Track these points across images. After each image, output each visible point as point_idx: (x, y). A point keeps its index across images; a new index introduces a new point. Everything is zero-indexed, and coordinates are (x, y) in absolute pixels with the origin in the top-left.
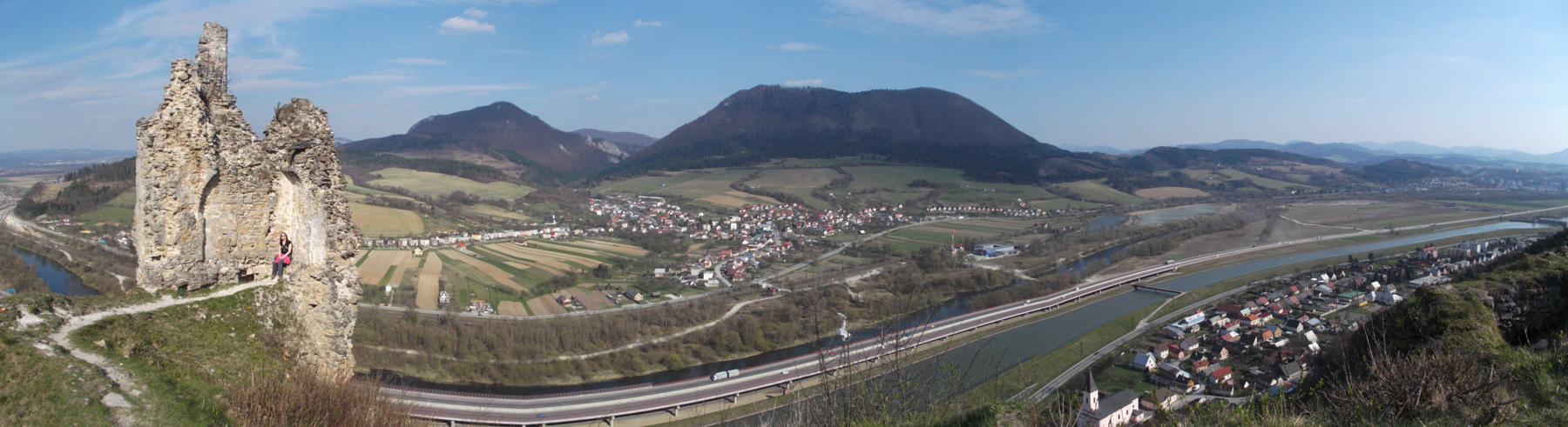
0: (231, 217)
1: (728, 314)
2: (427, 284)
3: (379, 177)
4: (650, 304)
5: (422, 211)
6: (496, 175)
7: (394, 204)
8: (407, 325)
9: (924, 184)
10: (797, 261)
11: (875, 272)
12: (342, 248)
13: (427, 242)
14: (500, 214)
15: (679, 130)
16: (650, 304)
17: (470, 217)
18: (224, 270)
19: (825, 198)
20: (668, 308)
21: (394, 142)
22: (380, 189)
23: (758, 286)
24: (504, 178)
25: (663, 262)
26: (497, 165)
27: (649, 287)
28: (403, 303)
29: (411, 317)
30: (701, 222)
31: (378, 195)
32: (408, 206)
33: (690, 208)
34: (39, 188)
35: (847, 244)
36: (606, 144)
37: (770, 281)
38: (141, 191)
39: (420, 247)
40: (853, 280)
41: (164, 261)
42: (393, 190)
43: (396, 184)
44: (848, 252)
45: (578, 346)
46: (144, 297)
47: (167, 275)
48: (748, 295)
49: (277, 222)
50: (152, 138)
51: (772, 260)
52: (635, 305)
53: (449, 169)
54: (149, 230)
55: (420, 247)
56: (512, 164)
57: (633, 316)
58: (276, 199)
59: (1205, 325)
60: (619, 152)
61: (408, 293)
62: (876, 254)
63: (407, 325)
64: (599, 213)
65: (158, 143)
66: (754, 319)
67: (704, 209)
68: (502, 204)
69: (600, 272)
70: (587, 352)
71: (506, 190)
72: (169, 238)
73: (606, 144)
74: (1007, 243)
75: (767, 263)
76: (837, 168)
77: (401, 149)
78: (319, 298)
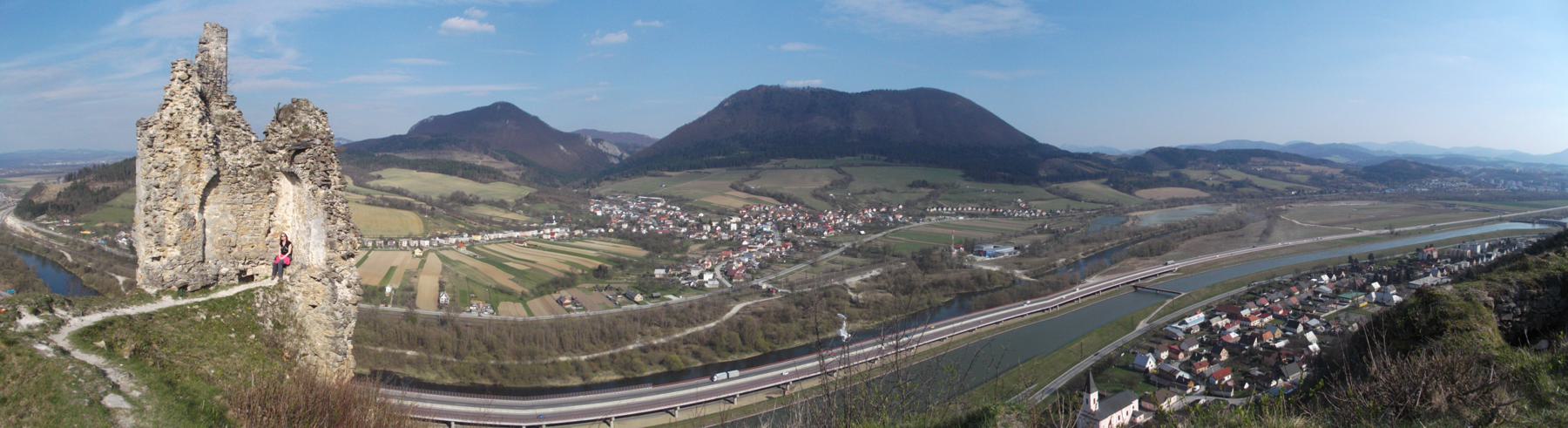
0: (231, 217)
1: (728, 315)
2: (427, 285)
3: (379, 177)
4: (650, 305)
5: (422, 211)
6: (496, 176)
7: (394, 205)
8: (406, 326)
9: (924, 184)
10: (797, 262)
11: (875, 272)
12: (342, 249)
13: (427, 243)
14: (500, 214)
15: (679, 130)
16: (650, 305)
17: (471, 218)
18: (224, 270)
19: (825, 199)
20: (668, 309)
21: (394, 143)
22: (380, 189)
23: (758, 287)
24: (505, 179)
25: (663, 262)
26: (497, 166)
27: (649, 288)
28: (403, 304)
29: (411, 318)
30: (701, 223)
31: (377, 195)
32: (408, 207)
33: (690, 209)
34: (38, 189)
35: (847, 245)
36: (606, 144)
37: (770, 282)
38: (141, 192)
39: (420, 247)
40: (853, 281)
41: (164, 261)
42: (393, 191)
43: (396, 184)
44: (848, 252)
45: (578, 347)
46: (144, 298)
47: (167, 275)
48: (748, 296)
49: (277, 222)
50: (152, 138)
51: (771, 260)
52: (635, 306)
53: (449, 169)
54: (149, 230)
55: (420, 247)
56: (512, 165)
57: (633, 317)
58: (276, 200)
59: (1205, 326)
60: (619, 153)
61: (408, 294)
62: (876, 255)
63: (406, 326)
64: (599, 213)
65: (158, 143)
66: (755, 320)
67: (705, 210)
68: (502, 205)
69: (600, 273)
70: (587, 352)
71: (506, 191)
72: (169, 239)
73: (606, 144)
74: (1007, 244)
75: (767, 264)
76: (837, 168)
77: (401, 150)
78: (319, 299)
